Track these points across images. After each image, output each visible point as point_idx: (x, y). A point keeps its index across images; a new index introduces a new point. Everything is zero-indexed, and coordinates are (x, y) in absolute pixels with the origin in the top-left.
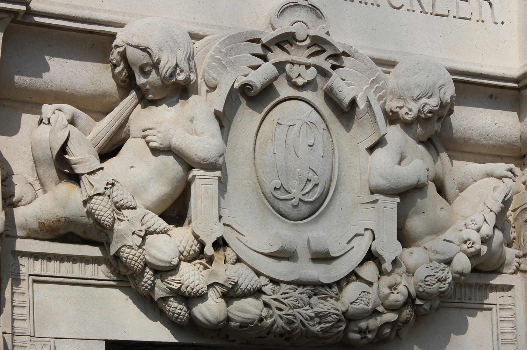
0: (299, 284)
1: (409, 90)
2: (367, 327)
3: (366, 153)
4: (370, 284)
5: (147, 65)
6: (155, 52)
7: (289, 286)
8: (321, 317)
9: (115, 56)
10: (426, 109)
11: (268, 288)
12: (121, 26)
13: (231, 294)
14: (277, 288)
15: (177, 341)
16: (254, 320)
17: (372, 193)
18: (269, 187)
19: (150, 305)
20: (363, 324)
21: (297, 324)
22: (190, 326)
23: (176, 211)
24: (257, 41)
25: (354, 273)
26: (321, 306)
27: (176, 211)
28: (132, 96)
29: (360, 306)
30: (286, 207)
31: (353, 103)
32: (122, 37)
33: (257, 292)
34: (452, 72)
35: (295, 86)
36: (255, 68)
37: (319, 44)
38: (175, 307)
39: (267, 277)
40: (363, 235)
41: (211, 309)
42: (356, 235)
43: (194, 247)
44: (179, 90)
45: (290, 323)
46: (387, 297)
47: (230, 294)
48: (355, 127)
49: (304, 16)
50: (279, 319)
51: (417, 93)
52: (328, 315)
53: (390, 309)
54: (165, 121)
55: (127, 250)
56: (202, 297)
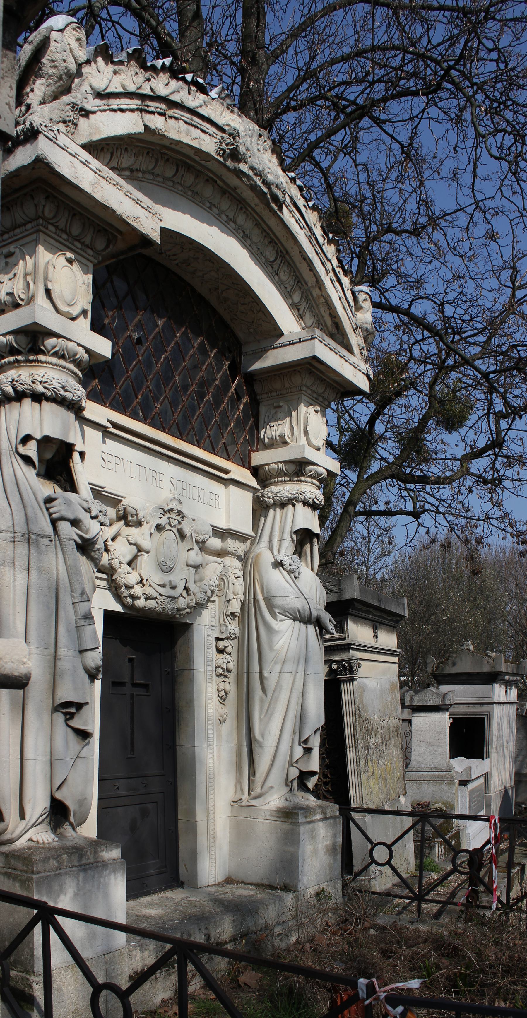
0: (168, 597)
6: (138, 511)
8: (173, 609)
11: (159, 597)
15: (122, 611)
19: (118, 598)
22: (132, 607)
28: (122, 522)
30: (164, 568)
32: (124, 502)
34: (212, 526)
35: (171, 526)
37: (180, 513)
38: (129, 600)
41: (141, 603)
44: (139, 524)
45: (163, 610)
47: (148, 598)
48: (184, 542)
49: (176, 502)
51: (203, 533)
53: (189, 608)
54: (134, 533)
56: (139, 598)
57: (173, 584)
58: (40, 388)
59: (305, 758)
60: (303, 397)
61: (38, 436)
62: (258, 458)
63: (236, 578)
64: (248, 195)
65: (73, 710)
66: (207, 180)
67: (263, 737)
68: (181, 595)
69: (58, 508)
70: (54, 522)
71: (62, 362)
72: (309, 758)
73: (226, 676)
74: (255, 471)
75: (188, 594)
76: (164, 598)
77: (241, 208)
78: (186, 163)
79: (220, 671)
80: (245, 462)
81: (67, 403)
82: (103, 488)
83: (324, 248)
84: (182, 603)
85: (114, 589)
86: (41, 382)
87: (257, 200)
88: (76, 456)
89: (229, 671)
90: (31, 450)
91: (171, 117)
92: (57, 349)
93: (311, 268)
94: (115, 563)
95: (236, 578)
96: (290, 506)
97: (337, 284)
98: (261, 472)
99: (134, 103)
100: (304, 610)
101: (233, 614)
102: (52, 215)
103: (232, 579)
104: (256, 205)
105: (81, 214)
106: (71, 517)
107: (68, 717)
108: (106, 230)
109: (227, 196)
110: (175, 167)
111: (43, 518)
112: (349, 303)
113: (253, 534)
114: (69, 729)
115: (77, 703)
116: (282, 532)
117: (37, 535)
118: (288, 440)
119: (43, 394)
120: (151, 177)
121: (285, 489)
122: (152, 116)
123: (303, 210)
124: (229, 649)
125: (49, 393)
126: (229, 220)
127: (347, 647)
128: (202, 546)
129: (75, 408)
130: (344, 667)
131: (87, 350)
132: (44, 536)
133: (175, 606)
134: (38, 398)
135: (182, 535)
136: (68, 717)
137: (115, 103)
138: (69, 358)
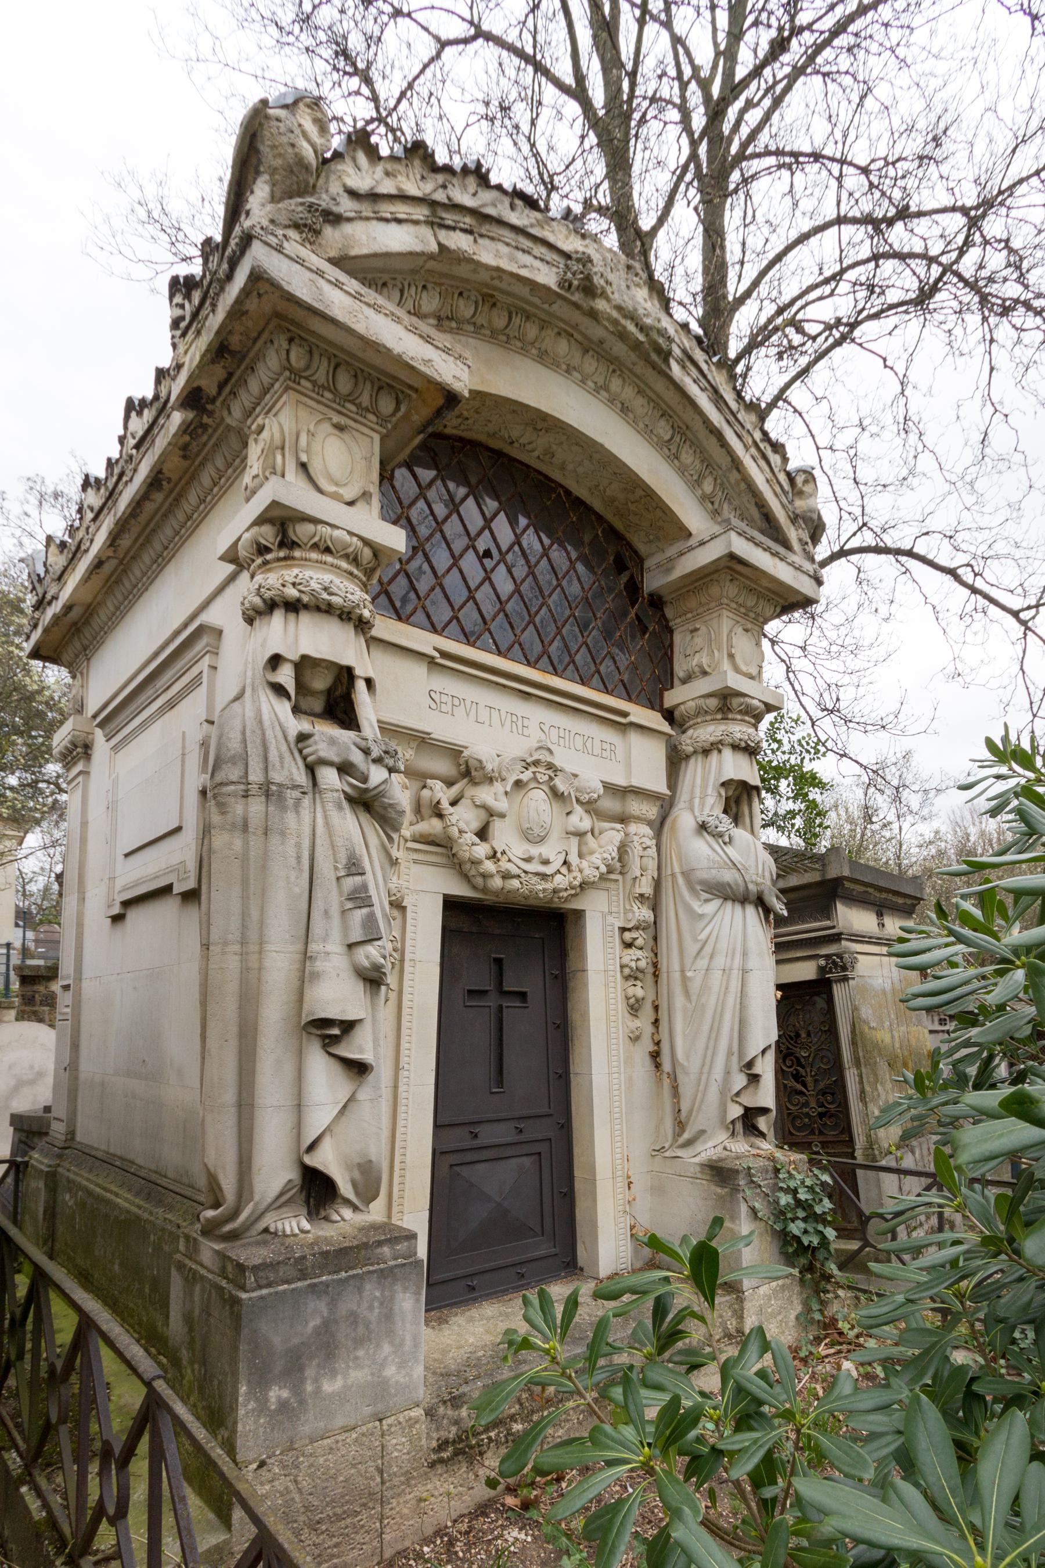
8: (544, 890)
11: (523, 875)
19: (466, 877)
22: (485, 890)
23: (482, 834)
27: (482, 834)
28: (465, 781)
30: (531, 837)
37: (550, 766)
41: (497, 882)
47: (506, 876)
56: (492, 876)
57: (544, 856)
58: (292, 592)
59: (751, 1089)
60: (725, 613)
61: (295, 656)
62: (670, 699)
63: (645, 849)
64: (619, 349)
65: (336, 1031)
66: (559, 334)
67: (688, 1060)
68: (559, 872)
69: (320, 748)
70: (311, 770)
71: (329, 559)
72: (757, 1088)
73: (636, 979)
74: (669, 715)
75: (569, 871)
77: (614, 371)
78: (524, 310)
79: (627, 971)
80: (654, 702)
83: (739, 416)
84: (560, 881)
86: (294, 584)
87: (633, 356)
88: (361, 686)
89: (642, 971)
90: (286, 676)
91: (482, 236)
92: (316, 539)
93: (723, 443)
94: (454, 832)
95: (645, 849)
96: (715, 753)
97: (762, 463)
98: (677, 713)
99: (420, 213)
100: (737, 885)
101: (642, 895)
102: (302, 364)
103: (638, 850)
104: (634, 364)
105: (348, 363)
106: (336, 759)
108: (392, 387)
109: (591, 353)
110: (506, 314)
111: (293, 764)
112: (781, 486)
113: (668, 792)
115: (342, 1022)
116: (704, 786)
117: (280, 785)
118: (708, 669)
119: (299, 600)
120: (471, 328)
121: (707, 732)
122: (452, 233)
123: (704, 367)
124: (640, 942)
125: (305, 599)
126: (598, 389)
127: (837, 938)
128: (590, 806)
129: (362, 626)
130: (834, 963)
132: (295, 787)
133: (549, 886)
134: (293, 607)
135: (556, 795)
137: (387, 209)
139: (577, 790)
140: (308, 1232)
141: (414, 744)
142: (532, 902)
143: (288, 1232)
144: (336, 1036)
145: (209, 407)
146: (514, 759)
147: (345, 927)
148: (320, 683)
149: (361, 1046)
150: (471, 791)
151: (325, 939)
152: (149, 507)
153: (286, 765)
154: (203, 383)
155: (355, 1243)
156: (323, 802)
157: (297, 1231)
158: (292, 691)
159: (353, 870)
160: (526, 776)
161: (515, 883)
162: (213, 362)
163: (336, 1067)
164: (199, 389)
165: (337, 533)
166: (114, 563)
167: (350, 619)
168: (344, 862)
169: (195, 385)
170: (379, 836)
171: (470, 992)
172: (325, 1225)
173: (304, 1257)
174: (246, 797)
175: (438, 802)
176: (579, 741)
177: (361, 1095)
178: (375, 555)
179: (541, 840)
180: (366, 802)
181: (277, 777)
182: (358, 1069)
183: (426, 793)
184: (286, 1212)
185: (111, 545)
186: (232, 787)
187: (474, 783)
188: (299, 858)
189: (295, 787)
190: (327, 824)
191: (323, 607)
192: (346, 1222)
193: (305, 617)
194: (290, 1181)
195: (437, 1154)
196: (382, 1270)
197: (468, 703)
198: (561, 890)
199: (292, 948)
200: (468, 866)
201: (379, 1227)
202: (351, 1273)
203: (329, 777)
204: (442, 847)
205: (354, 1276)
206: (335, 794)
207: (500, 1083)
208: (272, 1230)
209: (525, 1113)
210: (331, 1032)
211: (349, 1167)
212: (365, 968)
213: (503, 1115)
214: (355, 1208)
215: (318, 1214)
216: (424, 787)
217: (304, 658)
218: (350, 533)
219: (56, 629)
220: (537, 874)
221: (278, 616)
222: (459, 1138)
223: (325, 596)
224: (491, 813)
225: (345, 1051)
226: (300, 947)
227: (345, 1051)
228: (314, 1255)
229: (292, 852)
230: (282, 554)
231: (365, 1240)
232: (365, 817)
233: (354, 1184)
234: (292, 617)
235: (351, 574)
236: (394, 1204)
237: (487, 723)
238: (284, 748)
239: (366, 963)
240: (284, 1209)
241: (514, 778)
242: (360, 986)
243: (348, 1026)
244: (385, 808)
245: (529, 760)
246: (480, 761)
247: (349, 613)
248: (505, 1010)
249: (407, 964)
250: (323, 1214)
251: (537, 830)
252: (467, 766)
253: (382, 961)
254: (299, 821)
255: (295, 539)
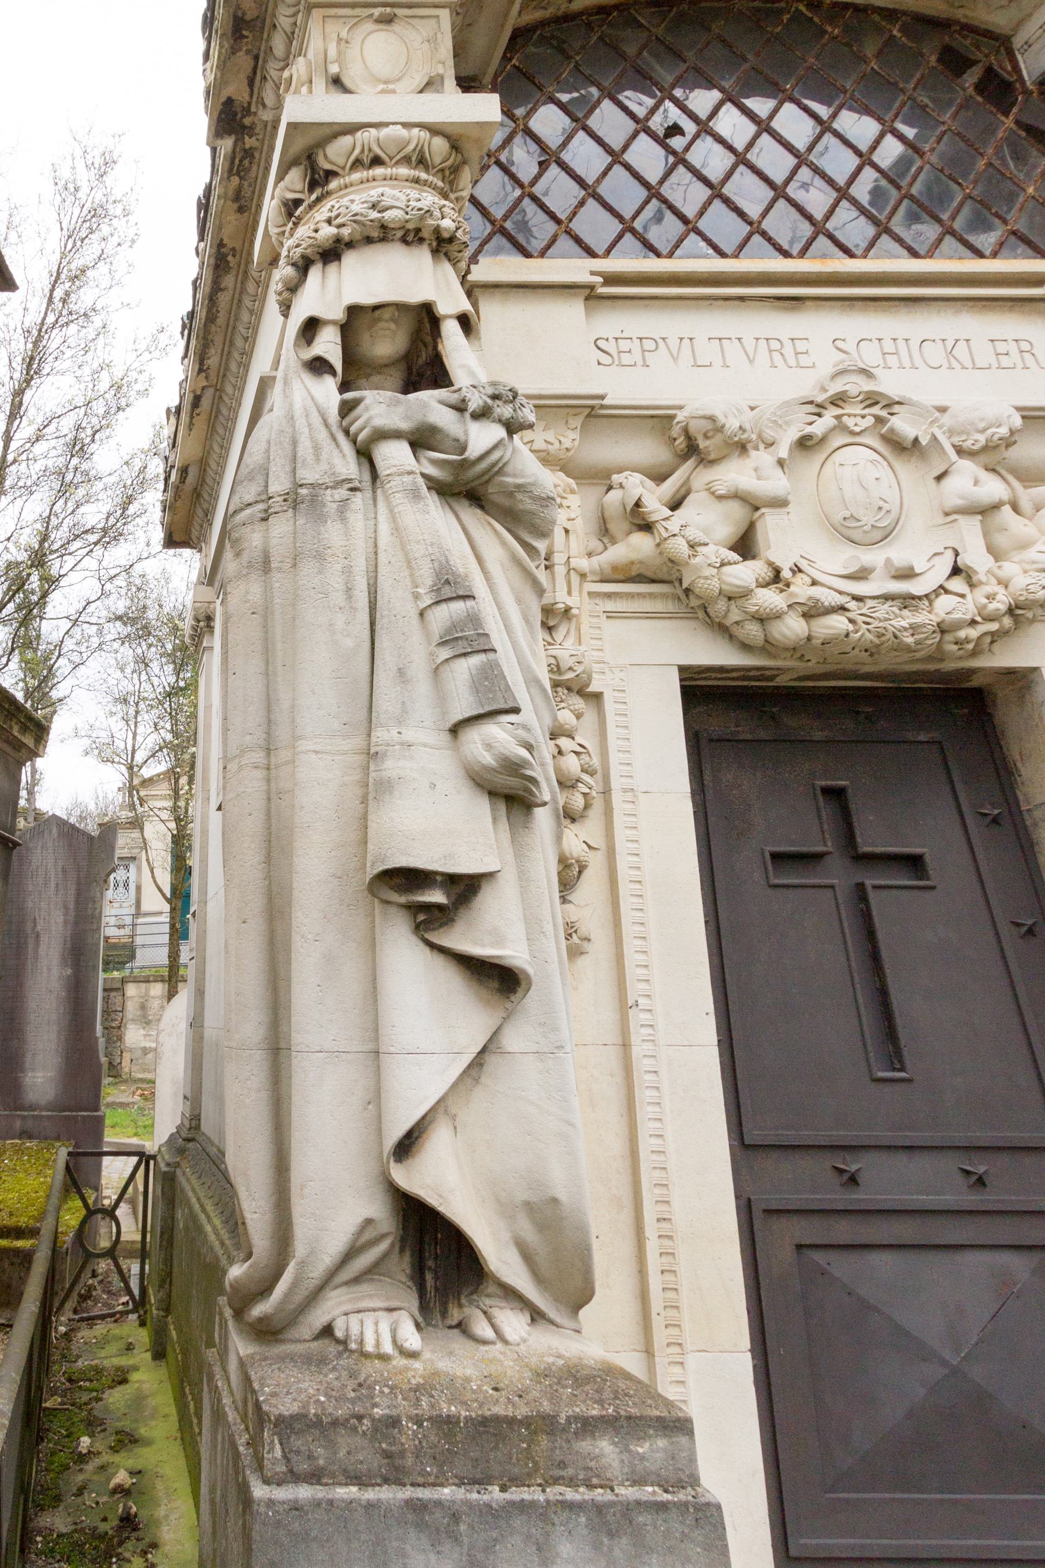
1: (972, 423)
2: (966, 638)
3: (933, 483)
4: (963, 596)
5: (708, 431)
7: (876, 601)
8: (914, 628)
9: (676, 431)
10: (996, 437)
11: (852, 605)
12: (681, 408)
13: (812, 613)
14: (861, 604)
16: (840, 635)
17: (947, 514)
18: (838, 518)
19: (722, 630)
20: (962, 634)
21: (889, 635)
22: (768, 647)
23: (745, 545)
24: (811, 402)
25: (941, 587)
26: (907, 619)
27: (745, 545)
28: (690, 463)
29: (957, 616)
30: (856, 535)
31: (916, 440)
32: (681, 416)
33: (843, 609)
36: (811, 424)
37: (872, 399)
39: (848, 594)
40: (942, 553)
41: (793, 627)
42: (936, 554)
43: (763, 575)
45: (880, 636)
46: (985, 606)
47: (812, 612)
50: (867, 634)
51: (981, 425)
52: (924, 625)
55: (702, 581)
56: (778, 616)
65: (437, 897)
70: (365, 454)
71: (379, 171)
75: (972, 585)
76: (870, 603)
81: (399, 234)
82: (603, 397)
85: (701, 614)
86: (329, 221)
88: (451, 329)
94: (679, 547)
106: (404, 426)
107: (421, 917)
111: (336, 452)
114: (439, 962)
119: (338, 240)
125: (346, 232)
128: (991, 454)
131: (434, 130)
136: (421, 917)
138: (391, 159)
139: (951, 432)
140: (413, 1355)
141: (577, 422)
142: (885, 663)
143: (369, 1347)
144: (440, 907)
145: (247, 121)
146: (787, 403)
147: (441, 697)
148: (386, 344)
149: (496, 929)
150: (703, 477)
151: (400, 720)
152: (224, 298)
153: (324, 456)
154: (229, 91)
155: (522, 1411)
156: (387, 499)
157: (388, 1348)
158: (338, 366)
159: (447, 592)
160: (819, 427)
161: (838, 623)
162: (234, 51)
163: (450, 979)
164: (229, 101)
165: (385, 132)
166: (209, 393)
167: (421, 240)
168: (429, 582)
169: (224, 99)
170: (504, 543)
171: (776, 857)
172: (458, 1343)
173: (394, 1422)
174: (265, 519)
175: (638, 504)
176: (935, 353)
177: (514, 1040)
178: (455, 146)
179: (886, 535)
180: (468, 488)
181: (308, 475)
182: (499, 980)
183: (614, 495)
184: (371, 1295)
185: (200, 371)
186: (248, 511)
187: (706, 461)
188: (349, 590)
189: (338, 484)
190: (397, 530)
191: (375, 234)
192: (503, 1353)
193: (350, 259)
194: (369, 1222)
195: (753, 1218)
196: (599, 1509)
197: (673, 343)
198: (958, 625)
199: (346, 745)
200: (721, 605)
201: (589, 1379)
202: (517, 1494)
203: (395, 456)
204: (663, 580)
205: (523, 1507)
206: (407, 479)
207: (895, 1057)
208: (339, 1334)
209: (982, 1136)
210: (428, 899)
211: (506, 1209)
212: (487, 769)
213: (924, 1137)
214: (536, 1316)
215: (444, 1314)
216: (610, 488)
217: (354, 311)
218: (405, 125)
219: (179, 503)
220: (887, 598)
221: (315, 274)
222: (806, 1181)
223: (374, 215)
224: (753, 504)
225: (463, 939)
226: (358, 742)
227: (463, 939)
228: (418, 1421)
229: (336, 582)
230: (314, 197)
231: (546, 1407)
232: (471, 516)
233: (527, 1257)
234: (332, 268)
235: (417, 181)
236: (657, 1323)
237: (718, 362)
238: (323, 435)
239: (488, 759)
240: (365, 1288)
241: (792, 434)
242: (483, 806)
243: (465, 888)
244: (511, 495)
245: (820, 399)
246: (712, 419)
247: (418, 230)
248: (873, 897)
249: (617, 798)
250: (455, 1315)
251: (868, 518)
252: (689, 437)
253: (524, 753)
254: (347, 534)
255: (328, 166)
